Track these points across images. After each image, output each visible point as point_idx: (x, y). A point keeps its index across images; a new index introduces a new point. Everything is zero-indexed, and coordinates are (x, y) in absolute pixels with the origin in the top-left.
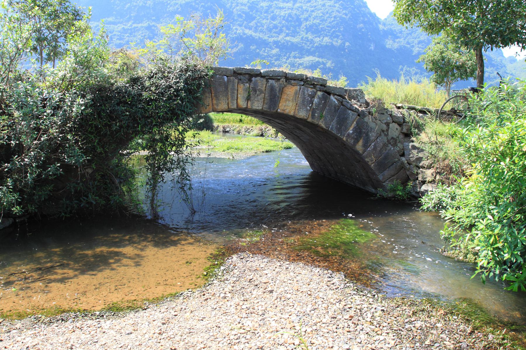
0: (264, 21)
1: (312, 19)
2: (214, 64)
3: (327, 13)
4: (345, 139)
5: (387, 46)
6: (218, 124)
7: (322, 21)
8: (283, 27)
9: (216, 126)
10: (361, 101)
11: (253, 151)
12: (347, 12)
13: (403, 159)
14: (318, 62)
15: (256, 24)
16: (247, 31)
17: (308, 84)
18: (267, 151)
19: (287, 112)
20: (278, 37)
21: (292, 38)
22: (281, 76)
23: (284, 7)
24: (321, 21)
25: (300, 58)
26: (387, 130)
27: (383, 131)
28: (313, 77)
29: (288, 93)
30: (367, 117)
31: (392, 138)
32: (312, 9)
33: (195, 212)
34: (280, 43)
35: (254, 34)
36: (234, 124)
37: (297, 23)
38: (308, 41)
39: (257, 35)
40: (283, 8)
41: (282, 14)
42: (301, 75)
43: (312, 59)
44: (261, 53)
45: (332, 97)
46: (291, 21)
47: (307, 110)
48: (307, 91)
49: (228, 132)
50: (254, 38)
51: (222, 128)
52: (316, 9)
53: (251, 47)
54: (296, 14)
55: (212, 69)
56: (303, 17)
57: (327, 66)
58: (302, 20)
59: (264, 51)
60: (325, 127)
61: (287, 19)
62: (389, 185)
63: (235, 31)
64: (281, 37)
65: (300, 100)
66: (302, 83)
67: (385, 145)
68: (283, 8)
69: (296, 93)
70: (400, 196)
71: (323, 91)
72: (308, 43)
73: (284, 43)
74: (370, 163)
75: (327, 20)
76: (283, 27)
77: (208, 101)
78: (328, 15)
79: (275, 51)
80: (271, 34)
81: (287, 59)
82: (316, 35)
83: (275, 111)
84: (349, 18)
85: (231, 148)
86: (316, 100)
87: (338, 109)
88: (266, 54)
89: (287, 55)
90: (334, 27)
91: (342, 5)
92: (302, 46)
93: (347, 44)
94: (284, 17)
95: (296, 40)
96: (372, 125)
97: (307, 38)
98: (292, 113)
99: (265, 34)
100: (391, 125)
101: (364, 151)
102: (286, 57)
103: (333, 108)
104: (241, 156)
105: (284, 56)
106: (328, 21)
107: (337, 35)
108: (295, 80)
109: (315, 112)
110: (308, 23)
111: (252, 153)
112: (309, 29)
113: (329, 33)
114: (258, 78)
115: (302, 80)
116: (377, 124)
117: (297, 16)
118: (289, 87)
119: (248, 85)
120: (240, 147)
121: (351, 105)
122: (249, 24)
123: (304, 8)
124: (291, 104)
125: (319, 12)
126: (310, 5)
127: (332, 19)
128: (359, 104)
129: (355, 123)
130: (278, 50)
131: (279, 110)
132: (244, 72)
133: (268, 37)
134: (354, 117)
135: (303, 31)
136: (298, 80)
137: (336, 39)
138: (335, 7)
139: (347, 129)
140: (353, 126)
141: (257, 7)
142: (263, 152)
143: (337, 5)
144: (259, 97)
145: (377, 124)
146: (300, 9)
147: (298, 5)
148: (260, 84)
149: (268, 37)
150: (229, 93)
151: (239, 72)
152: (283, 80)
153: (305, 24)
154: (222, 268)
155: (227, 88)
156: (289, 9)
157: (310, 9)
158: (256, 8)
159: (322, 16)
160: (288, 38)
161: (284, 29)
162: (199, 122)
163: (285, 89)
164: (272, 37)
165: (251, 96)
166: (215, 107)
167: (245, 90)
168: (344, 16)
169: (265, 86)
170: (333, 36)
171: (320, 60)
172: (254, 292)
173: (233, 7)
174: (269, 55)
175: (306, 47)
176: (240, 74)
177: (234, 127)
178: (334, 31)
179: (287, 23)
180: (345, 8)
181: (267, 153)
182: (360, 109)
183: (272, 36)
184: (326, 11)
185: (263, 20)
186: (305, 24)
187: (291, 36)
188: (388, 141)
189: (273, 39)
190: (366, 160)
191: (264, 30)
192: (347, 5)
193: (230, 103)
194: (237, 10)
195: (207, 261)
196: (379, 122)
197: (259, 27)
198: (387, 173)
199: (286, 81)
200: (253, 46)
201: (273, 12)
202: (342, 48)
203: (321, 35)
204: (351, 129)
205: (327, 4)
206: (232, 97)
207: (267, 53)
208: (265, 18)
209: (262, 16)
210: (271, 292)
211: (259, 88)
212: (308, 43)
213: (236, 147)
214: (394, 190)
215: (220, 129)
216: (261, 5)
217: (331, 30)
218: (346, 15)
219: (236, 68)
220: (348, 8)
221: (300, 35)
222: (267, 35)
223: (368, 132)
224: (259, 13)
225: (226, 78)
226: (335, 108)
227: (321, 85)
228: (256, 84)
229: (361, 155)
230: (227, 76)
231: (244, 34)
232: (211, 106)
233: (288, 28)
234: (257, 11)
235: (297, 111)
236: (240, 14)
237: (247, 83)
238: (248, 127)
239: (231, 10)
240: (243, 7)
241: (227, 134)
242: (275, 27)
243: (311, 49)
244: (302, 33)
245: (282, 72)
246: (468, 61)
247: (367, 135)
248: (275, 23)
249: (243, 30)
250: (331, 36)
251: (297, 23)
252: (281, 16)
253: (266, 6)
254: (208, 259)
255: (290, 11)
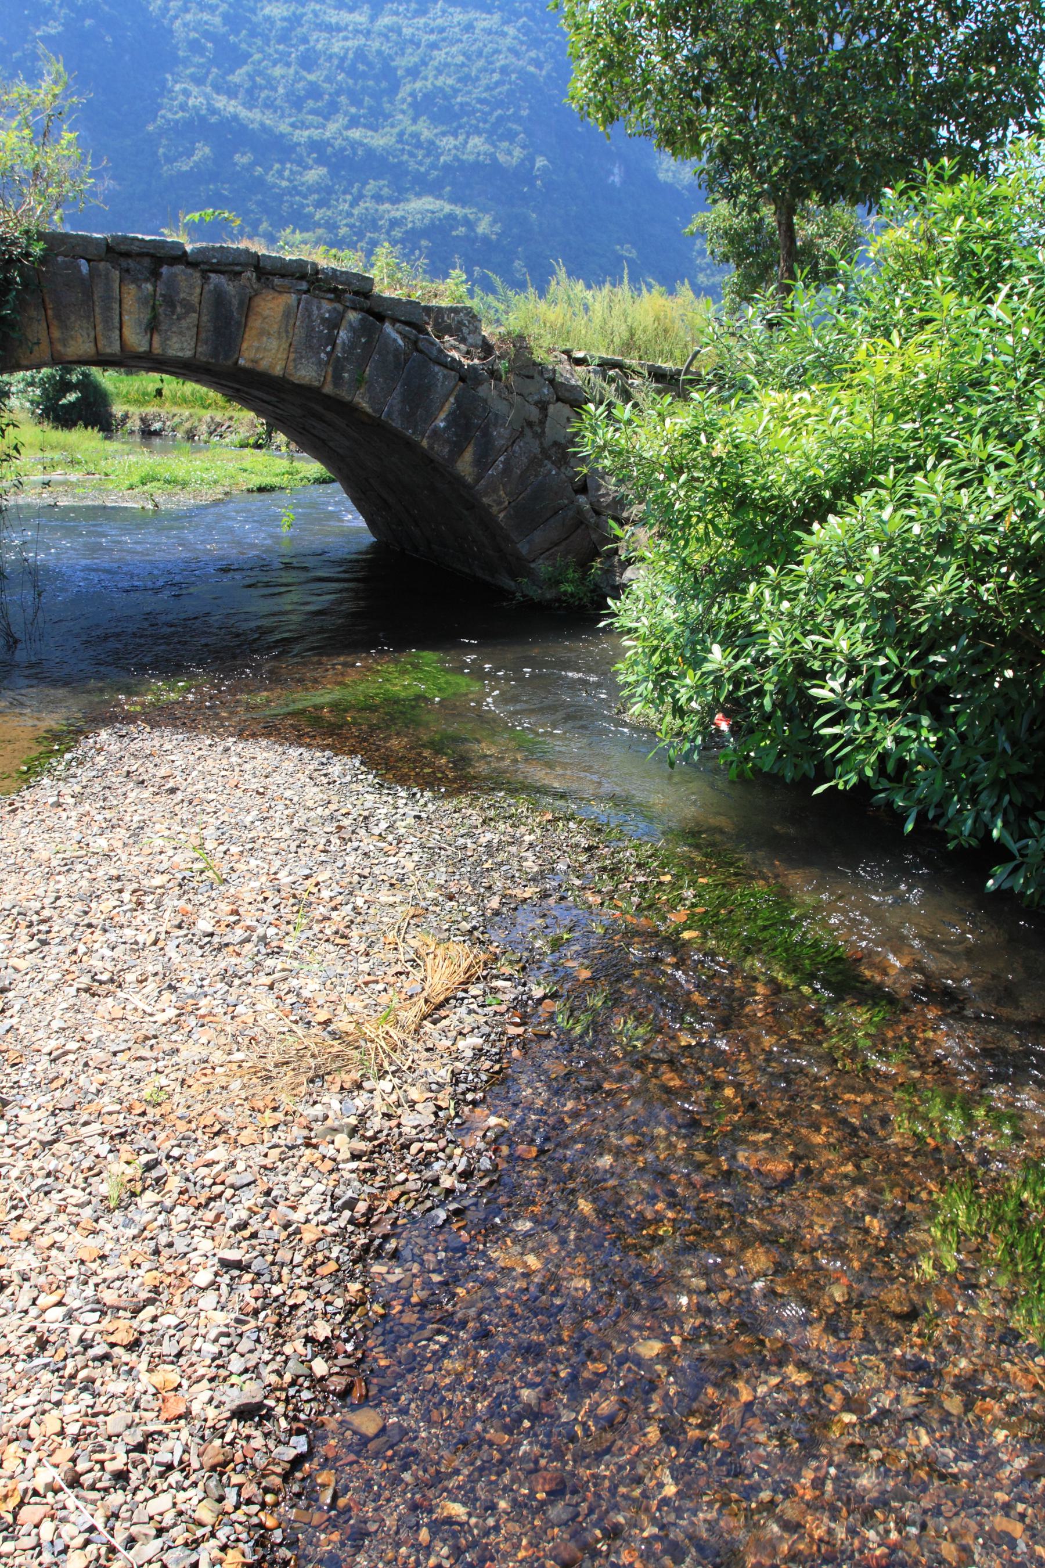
0: (278, 71)
1: (431, 75)
2: (51, 222)
3: (480, 54)
4: (425, 443)
5: (661, 176)
6: (125, 408)
7: (465, 79)
8: (338, 93)
9: (119, 415)
10: (471, 339)
11: (220, 489)
12: (542, 58)
13: (582, 499)
14: (451, 216)
15: (251, 78)
16: (221, 102)
17: (320, 289)
18: (261, 490)
19: (264, 365)
20: (324, 127)
21: (370, 133)
22: (245, 265)
23: (342, 24)
24: (459, 80)
25: (395, 201)
26: (542, 423)
27: (530, 424)
28: (334, 270)
29: (266, 313)
30: (486, 385)
31: (556, 443)
32: (433, 37)
33: (16, 641)
34: (329, 150)
35: (244, 113)
36: (175, 410)
37: (384, 85)
38: (419, 145)
39: (254, 117)
40: (339, 29)
41: (336, 50)
42: (301, 264)
43: (431, 207)
44: (270, 178)
45: (388, 327)
46: (364, 76)
47: (320, 362)
48: (319, 308)
49: (157, 433)
50: (243, 128)
51: (138, 423)
52: (444, 40)
53: (237, 156)
54: (379, 53)
55: (41, 236)
56: (402, 63)
57: (480, 230)
58: (400, 73)
59: (280, 174)
60: (369, 410)
61: (353, 66)
62: (543, 568)
63: (181, 98)
64: (332, 127)
65: (300, 333)
66: (304, 286)
67: (535, 463)
68: (339, 29)
69: (287, 314)
70: (572, 595)
71: (362, 310)
72: (420, 154)
73: (344, 149)
74: (495, 509)
75: (478, 78)
76: (338, 93)
77: (37, 331)
78: (481, 63)
79: (315, 175)
80: (300, 117)
81: (354, 203)
82: (444, 128)
83: (230, 363)
84: (549, 76)
85: (155, 479)
86: (343, 335)
87: (406, 361)
88: (284, 184)
89: (355, 190)
90: (499, 104)
91: (526, 30)
92: (401, 163)
93: (541, 162)
94: (343, 59)
95: (381, 142)
96: (499, 406)
97: (416, 135)
98: (278, 371)
99: (282, 116)
100: (551, 409)
101: (479, 478)
102: (349, 197)
103: (391, 358)
104: (184, 500)
105: (344, 193)
106: (484, 82)
107: (510, 130)
108: (283, 276)
109: (343, 369)
110: (418, 85)
111: (218, 492)
112: (422, 106)
113: (485, 122)
114: (179, 268)
115: (303, 277)
116: (511, 405)
117: (386, 60)
118: (270, 295)
119: (149, 286)
120: (181, 474)
121: (441, 351)
122: (230, 78)
123: (407, 32)
124: (274, 344)
125: (454, 49)
126: (426, 25)
127: (496, 77)
128: (462, 347)
129: (452, 400)
130: (323, 171)
131: (241, 362)
132: (135, 248)
133: (293, 125)
134: (449, 384)
135: (403, 112)
136: (292, 275)
137: (505, 144)
138: (504, 35)
139: (432, 417)
140: (447, 408)
141: (254, 19)
142: (250, 491)
143: (511, 30)
144: (184, 323)
145: (511, 405)
146: (393, 36)
147: (385, 20)
148: (183, 284)
149: (293, 125)
150: (97, 310)
151: (123, 248)
152: (250, 274)
153: (408, 88)
154: (68, 756)
155: (89, 294)
156: (357, 32)
157: (427, 38)
158: (249, 21)
159: (463, 65)
160: (356, 134)
161: (343, 99)
162: (64, 401)
163: (257, 300)
164: (304, 126)
165: (162, 318)
166: (59, 347)
167: (143, 301)
168: (532, 69)
169: (198, 290)
170: (497, 133)
171: (459, 211)
172: (132, 796)
173: (172, 13)
174: (295, 188)
175: (412, 166)
176: (127, 255)
177: (176, 420)
178: (500, 119)
179: (351, 82)
180: (536, 43)
181: (265, 496)
182: (466, 362)
183: (303, 123)
184: (474, 48)
185: (275, 65)
186: (408, 88)
187: (365, 126)
188: (544, 451)
189: (306, 133)
190: (485, 500)
191: (278, 102)
192: (543, 32)
193: (100, 337)
194: (185, 25)
195: (34, 745)
196: (517, 399)
197: (262, 88)
198: (539, 537)
199: (259, 279)
200: (244, 154)
201: (305, 40)
202: (524, 174)
203: (460, 127)
204: (442, 415)
205: (480, 25)
206: (107, 320)
207: (289, 180)
208: (279, 61)
209: (271, 51)
210: (173, 791)
211: (182, 295)
212: (420, 154)
213: (167, 475)
214: (555, 582)
215: (134, 424)
216: (267, 11)
217: (490, 113)
218: (539, 65)
219: (114, 238)
220: (544, 42)
221: (392, 126)
222: (288, 120)
223: (487, 426)
224: (259, 42)
225: (84, 266)
226: (396, 356)
227: (356, 293)
228: (172, 284)
229: (469, 487)
230: (89, 261)
231: (213, 111)
232: (45, 346)
233: (357, 102)
234: (253, 34)
235: (291, 365)
236: (196, 41)
237: (147, 280)
238: (218, 419)
239: (166, 22)
240: (206, 17)
241: (157, 441)
242: (314, 92)
243: (427, 173)
244: (400, 117)
245: (247, 251)
246: (821, 237)
247: (486, 434)
248: (311, 77)
249: (208, 98)
250: (491, 133)
251: (384, 85)
252: (330, 58)
253: (284, 19)
254: (38, 740)
255: (361, 40)
